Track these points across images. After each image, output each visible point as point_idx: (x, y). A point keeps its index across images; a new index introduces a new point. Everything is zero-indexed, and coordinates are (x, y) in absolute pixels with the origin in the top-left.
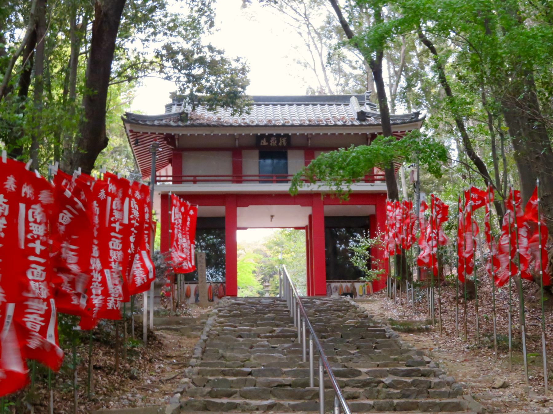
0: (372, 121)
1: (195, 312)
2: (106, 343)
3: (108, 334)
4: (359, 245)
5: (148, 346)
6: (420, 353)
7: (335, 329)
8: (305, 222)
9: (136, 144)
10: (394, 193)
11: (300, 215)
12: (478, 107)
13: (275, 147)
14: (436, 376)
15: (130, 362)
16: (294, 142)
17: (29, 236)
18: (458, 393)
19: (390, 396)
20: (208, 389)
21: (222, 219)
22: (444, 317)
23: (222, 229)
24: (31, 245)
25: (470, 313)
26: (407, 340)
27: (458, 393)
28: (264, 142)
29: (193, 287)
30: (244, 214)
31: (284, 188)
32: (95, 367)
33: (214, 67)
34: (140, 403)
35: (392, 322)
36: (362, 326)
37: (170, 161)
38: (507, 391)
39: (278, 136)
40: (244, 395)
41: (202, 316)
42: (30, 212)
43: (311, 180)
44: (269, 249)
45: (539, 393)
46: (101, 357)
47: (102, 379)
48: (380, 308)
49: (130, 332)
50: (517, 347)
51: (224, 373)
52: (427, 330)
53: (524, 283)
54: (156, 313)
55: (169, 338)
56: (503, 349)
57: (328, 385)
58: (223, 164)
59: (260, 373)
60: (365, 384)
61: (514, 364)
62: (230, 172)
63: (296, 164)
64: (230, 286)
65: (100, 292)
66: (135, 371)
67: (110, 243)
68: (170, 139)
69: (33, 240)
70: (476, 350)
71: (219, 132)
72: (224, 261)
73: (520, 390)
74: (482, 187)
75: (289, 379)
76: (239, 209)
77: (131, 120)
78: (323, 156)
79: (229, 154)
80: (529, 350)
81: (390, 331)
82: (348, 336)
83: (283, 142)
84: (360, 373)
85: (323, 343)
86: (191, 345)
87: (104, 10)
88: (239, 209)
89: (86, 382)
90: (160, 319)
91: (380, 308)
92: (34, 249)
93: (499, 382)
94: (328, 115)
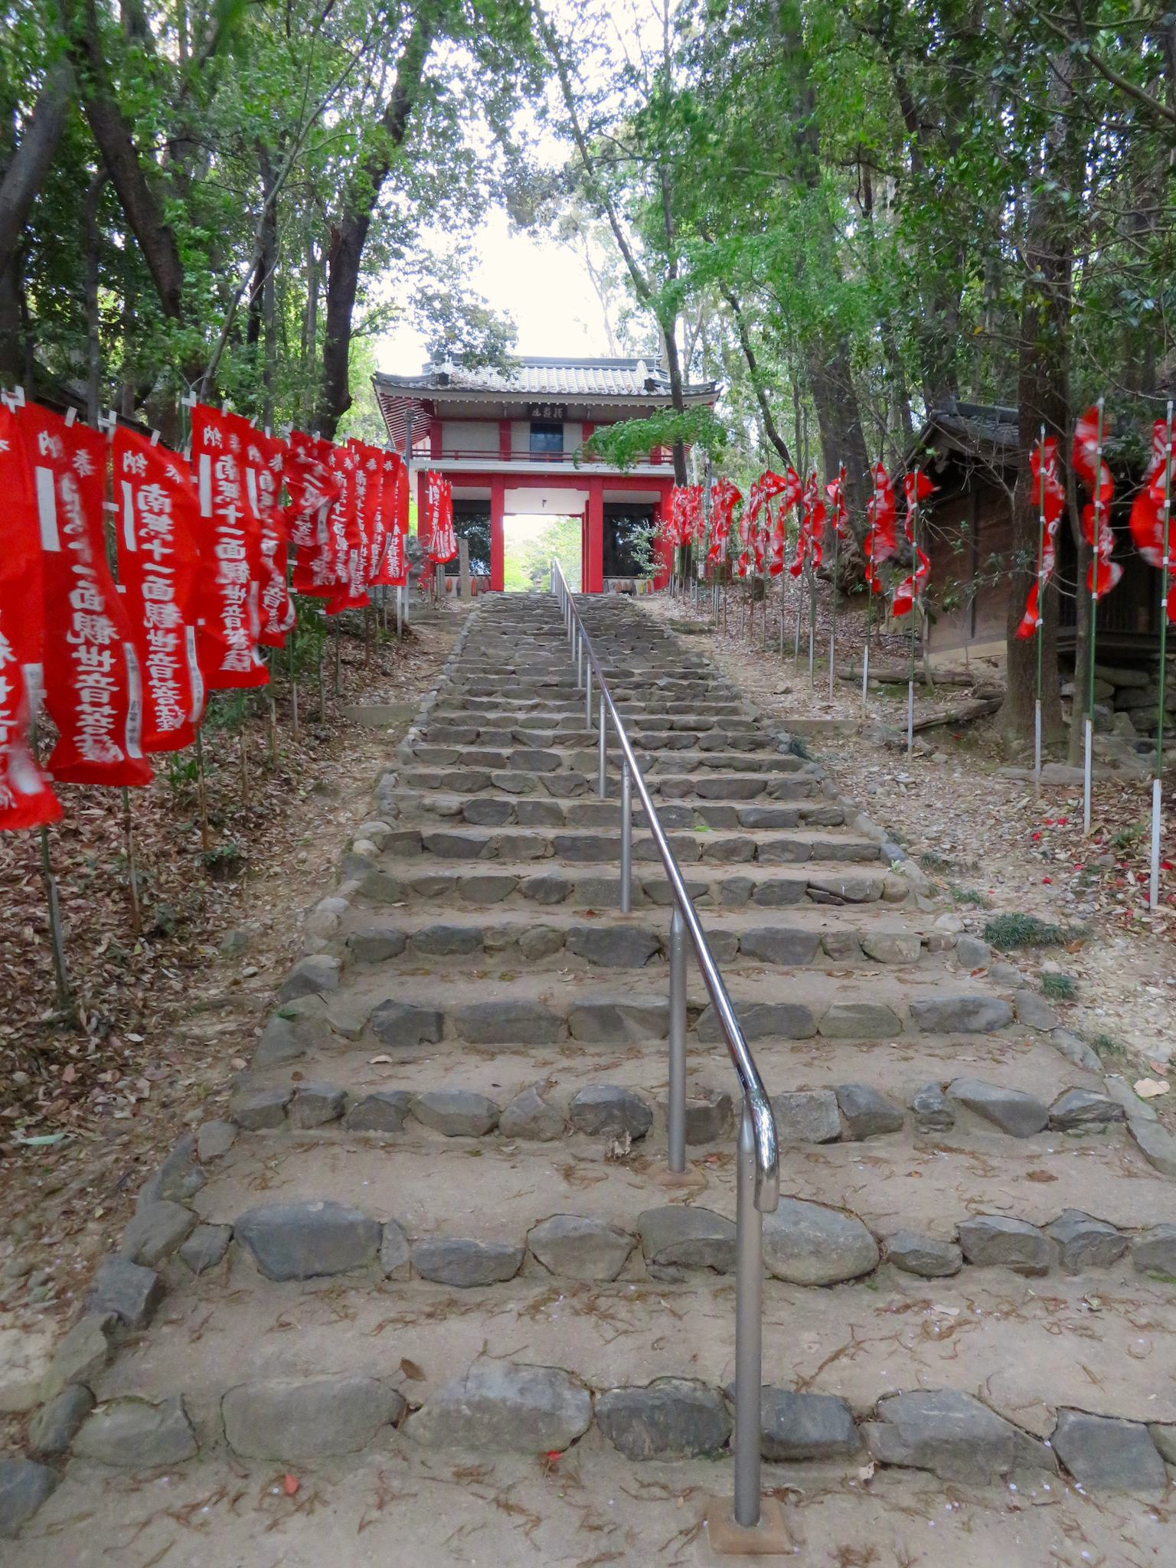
0: (662, 391)
1: (456, 606)
2: (356, 636)
3: (358, 627)
4: (640, 534)
5: (403, 640)
6: (700, 655)
7: (608, 628)
8: (581, 509)
9: (389, 409)
10: (681, 478)
11: (575, 500)
12: (784, 380)
13: (548, 419)
14: (715, 679)
15: (383, 657)
16: (571, 413)
17: (218, 499)
18: (736, 697)
19: (663, 699)
20: (466, 688)
21: (487, 503)
22: (729, 618)
23: (487, 514)
25: (758, 614)
26: (687, 641)
27: (736, 697)
28: (536, 413)
29: (455, 579)
30: (513, 498)
31: (566, 468)
32: (343, 662)
33: (475, 317)
34: (393, 700)
35: (672, 622)
36: (638, 625)
37: (428, 433)
38: (790, 697)
39: (553, 406)
40: (506, 695)
41: (464, 611)
43: (590, 459)
44: (541, 539)
45: (822, 699)
46: (351, 651)
47: (352, 676)
48: (661, 607)
49: (382, 624)
50: (804, 651)
51: (485, 671)
52: (710, 631)
54: (412, 606)
55: (425, 633)
56: (789, 653)
57: (596, 686)
58: (490, 438)
59: (525, 672)
60: (638, 686)
61: (799, 668)
62: (497, 448)
63: (572, 439)
64: (495, 581)
65: (169, 673)
66: (388, 667)
68: (427, 406)
69: (149, 539)
70: (760, 654)
71: (467, 398)
72: (489, 551)
73: (803, 696)
74: (781, 472)
75: (555, 679)
77: (379, 380)
78: (601, 431)
79: (495, 425)
80: (817, 655)
81: (668, 631)
82: (623, 635)
83: (559, 413)
84: (632, 674)
85: (594, 644)
86: (450, 641)
87: (343, 235)
89: (334, 676)
90: (416, 614)
91: (661, 607)
92: (150, 552)
93: (781, 688)
94: (611, 383)
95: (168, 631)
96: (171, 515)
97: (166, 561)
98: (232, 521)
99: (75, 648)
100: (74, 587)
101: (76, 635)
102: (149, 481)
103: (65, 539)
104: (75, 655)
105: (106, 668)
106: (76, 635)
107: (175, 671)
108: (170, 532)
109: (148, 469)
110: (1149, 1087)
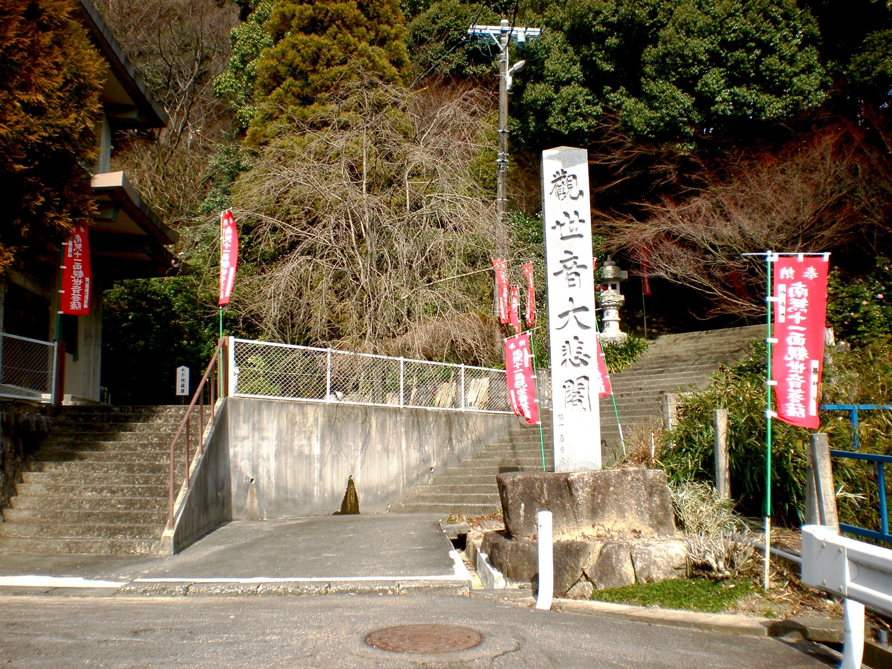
17: (789, 310)
69: (794, 312)
92: (793, 320)
95: (801, 362)
96: (807, 298)
98: (798, 322)
99: (788, 362)
101: (789, 356)
102: (795, 281)
104: (788, 365)
105: (801, 372)
106: (789, 356)
107: (802, 384)
108: (806, 307)
109: (795, 275)
110: (91, 202)
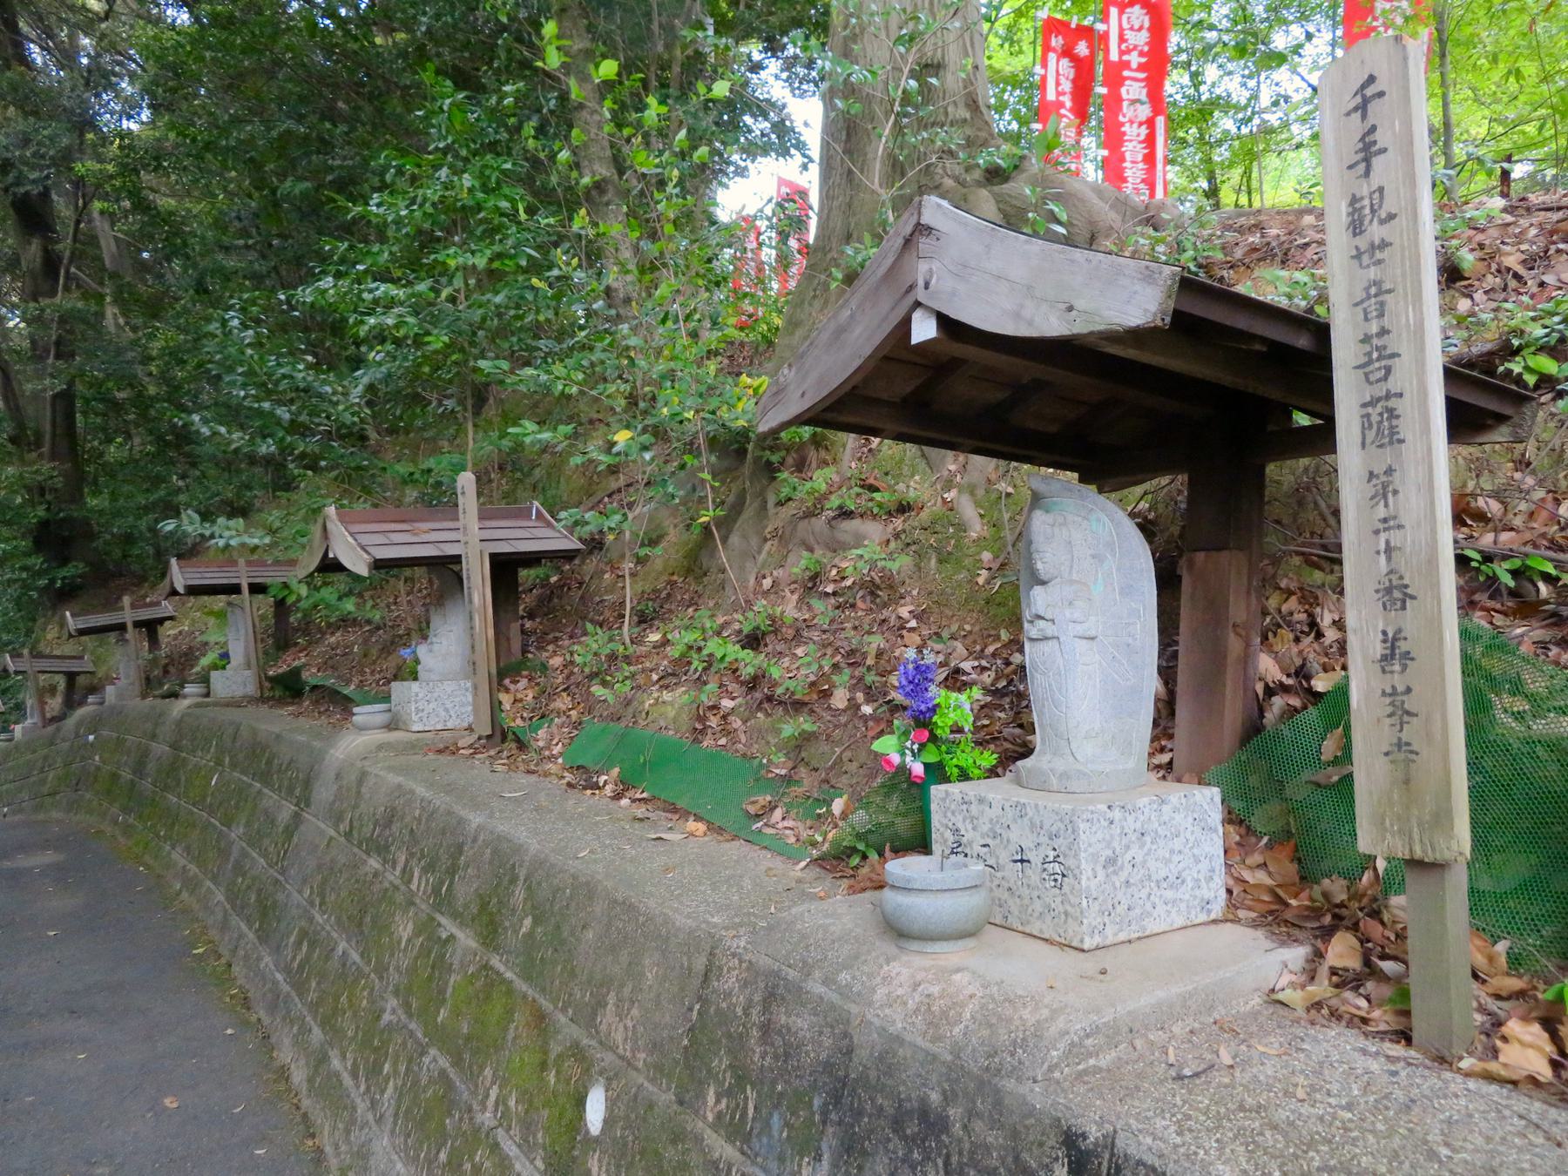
17: (1123, 47)
24: (1125, 58)
42: (1125, 17)
53: (213, 35)
65: (1140, 158)
67: (1123, 90)
69: (1128, 52)
76: (1214, 793)
88: (1214, 793)
92: (1128, 63)
97: (1141, 68)
100: (1122, 85)
103: (1059, 94)
105: (1142, 137)
